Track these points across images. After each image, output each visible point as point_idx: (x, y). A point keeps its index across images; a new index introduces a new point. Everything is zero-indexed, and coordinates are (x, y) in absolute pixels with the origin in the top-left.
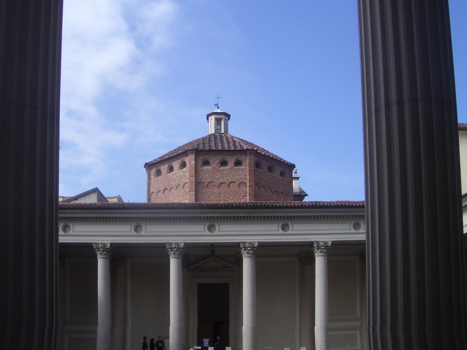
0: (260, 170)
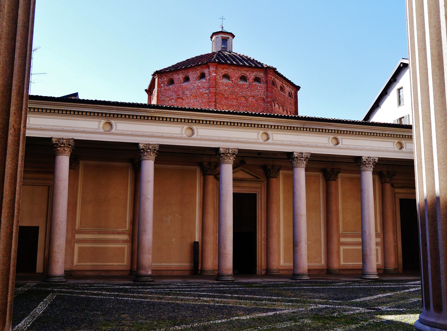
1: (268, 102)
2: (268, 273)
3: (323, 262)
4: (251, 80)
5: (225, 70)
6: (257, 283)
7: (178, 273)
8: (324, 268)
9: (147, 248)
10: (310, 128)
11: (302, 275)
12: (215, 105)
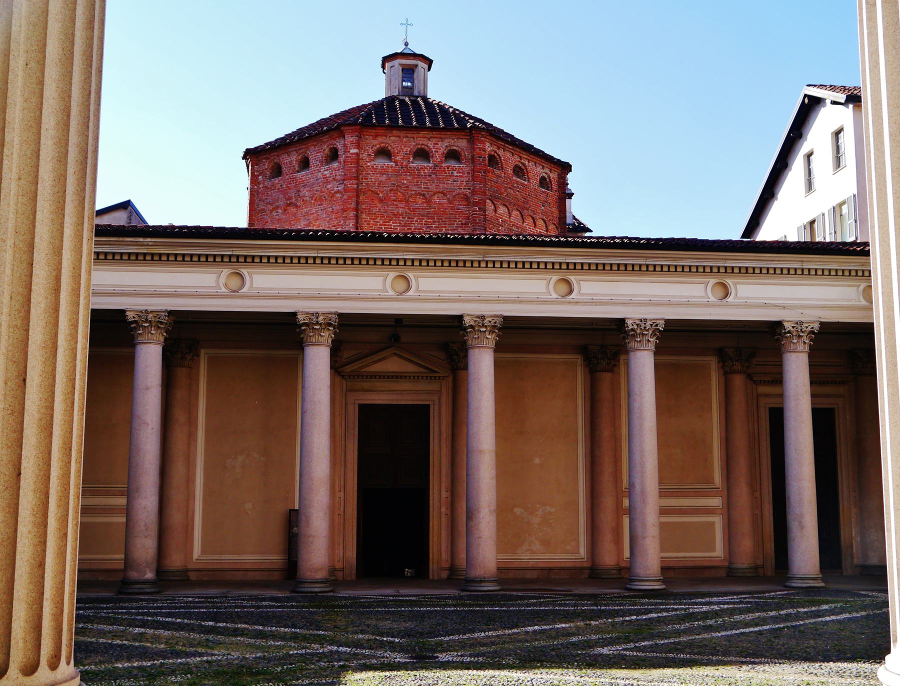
0: (497, 172)
1: (476, 204)
2: (458, 577)
3: (583, 552)
4: (438, 157)
5: (380, 139)
6: (446, 598)
7: (258, 576)
8: (585, 565)
9: (142, 524)
10: (501, 262)
11: (481, 582)
12: (357, 217)
